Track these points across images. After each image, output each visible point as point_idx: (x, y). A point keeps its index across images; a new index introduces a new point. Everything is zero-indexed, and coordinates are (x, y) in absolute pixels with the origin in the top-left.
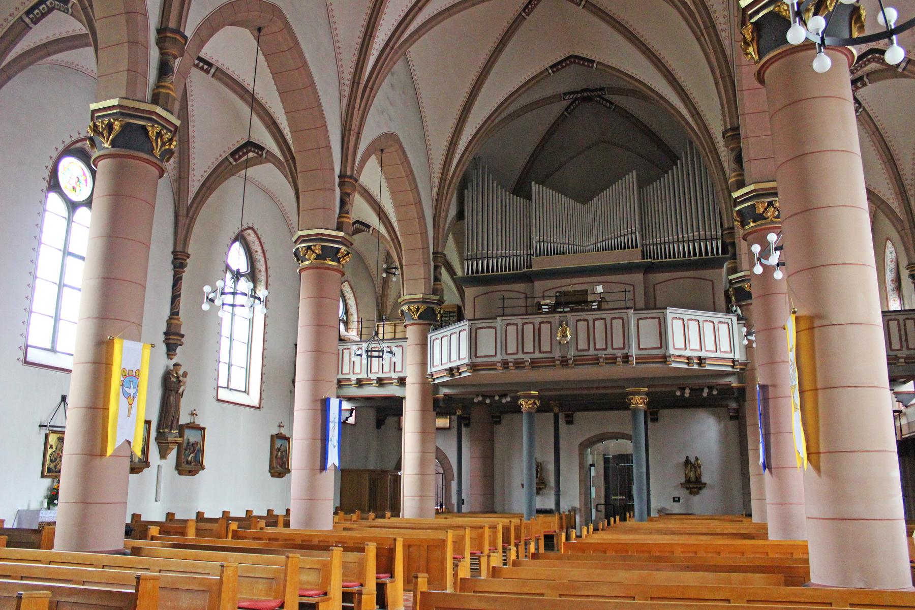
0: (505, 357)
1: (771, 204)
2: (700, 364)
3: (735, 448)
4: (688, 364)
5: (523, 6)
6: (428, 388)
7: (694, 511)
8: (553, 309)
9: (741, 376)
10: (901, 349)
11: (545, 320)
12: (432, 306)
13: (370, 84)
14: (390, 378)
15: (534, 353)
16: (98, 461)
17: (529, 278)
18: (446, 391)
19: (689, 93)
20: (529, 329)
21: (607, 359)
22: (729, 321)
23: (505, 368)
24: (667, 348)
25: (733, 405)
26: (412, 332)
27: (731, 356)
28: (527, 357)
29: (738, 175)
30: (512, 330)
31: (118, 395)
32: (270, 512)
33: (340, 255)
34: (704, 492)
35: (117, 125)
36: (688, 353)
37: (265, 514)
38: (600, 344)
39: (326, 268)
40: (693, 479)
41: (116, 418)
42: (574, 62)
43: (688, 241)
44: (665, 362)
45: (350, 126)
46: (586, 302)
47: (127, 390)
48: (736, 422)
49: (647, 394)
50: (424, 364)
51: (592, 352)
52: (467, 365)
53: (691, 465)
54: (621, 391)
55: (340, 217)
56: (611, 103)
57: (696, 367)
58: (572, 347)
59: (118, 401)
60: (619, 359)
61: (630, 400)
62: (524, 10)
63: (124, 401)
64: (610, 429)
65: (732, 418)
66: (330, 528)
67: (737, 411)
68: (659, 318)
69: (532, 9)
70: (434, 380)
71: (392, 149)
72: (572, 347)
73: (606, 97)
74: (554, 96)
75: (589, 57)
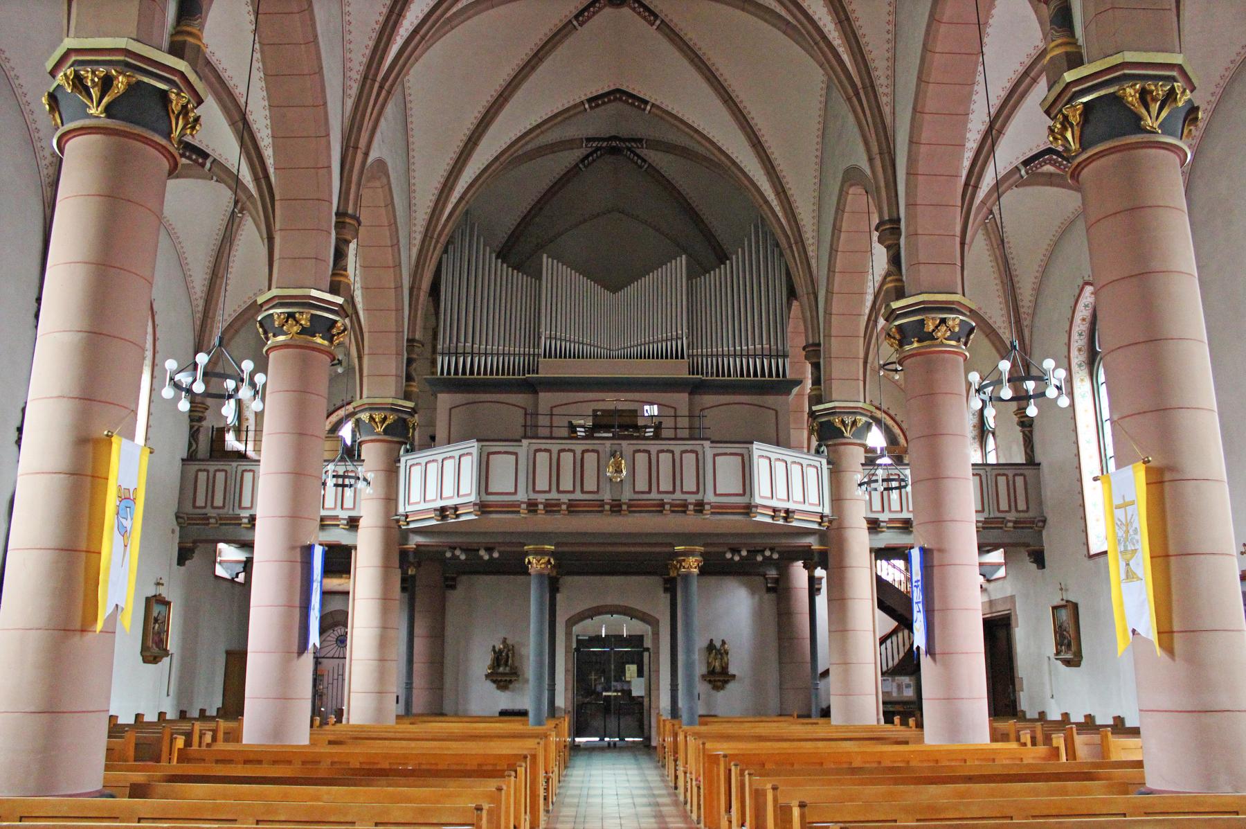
0: (533, 496)
1: (943, 321)
2: (786, 519)
3: (772, 630)
4: (773, 517)
5: (575, 12)
6: (395, 532)
7: (718, 712)
8: (590, 434)
9: (822, 536)
10: (1009, 511)
11: (590, 447)
12: (405, 416)
13: (388, 84)
14: (336, 518)
15: (573, 492)
16: (76, 639)
17: (532, 387)
18: (420, 539)
19: (775, 163)
20: (567, 458)
21: (672, 505)
22: (818, 464)
23: (530, 511)
24: (751, 495)
25: (772, 573)
26: (371, 453)
27: (819, 509)
28: (564, 498)
29: (897, 280)
30: (542, 458)
31: (112, 529)
32: (138, 717)
33: (335, 331)
34: (731, 686)
35: (121, 83)
36: (774, 503)
37: (1111, 722)
38: (665, 485)
39: (313, 349)
40: (718, 669)
41: (108, 569)
42: (620, 99)
43: (748, 356)
44: (747, 514)
45: (357, 140)
46: (636, 427)
47: (123, 521)
48: (773, 596)
49: (702, 554)
50: (390, 498)
51: (654, 495)
52: (475, 504)
53: (716, 651)
54: (670, 549)
55: (333, 275)
56: (644, 161)
57: (781, 522)
58: (627, 489)
59: (111, 540)
60: (691, 507)
61: (680, 562)
62: (576, 17)
63: (118, 538)
64: (610, 601)
65: (769, 590)
66: (307, 742)
67: (777, 581)
68: (742, 455)
69: (589, 18)
70: (408, 523)
71: (378, 184)
72: (627, 489)
73: (638, 151)
74: (572, 140)
75: (641, 96)
